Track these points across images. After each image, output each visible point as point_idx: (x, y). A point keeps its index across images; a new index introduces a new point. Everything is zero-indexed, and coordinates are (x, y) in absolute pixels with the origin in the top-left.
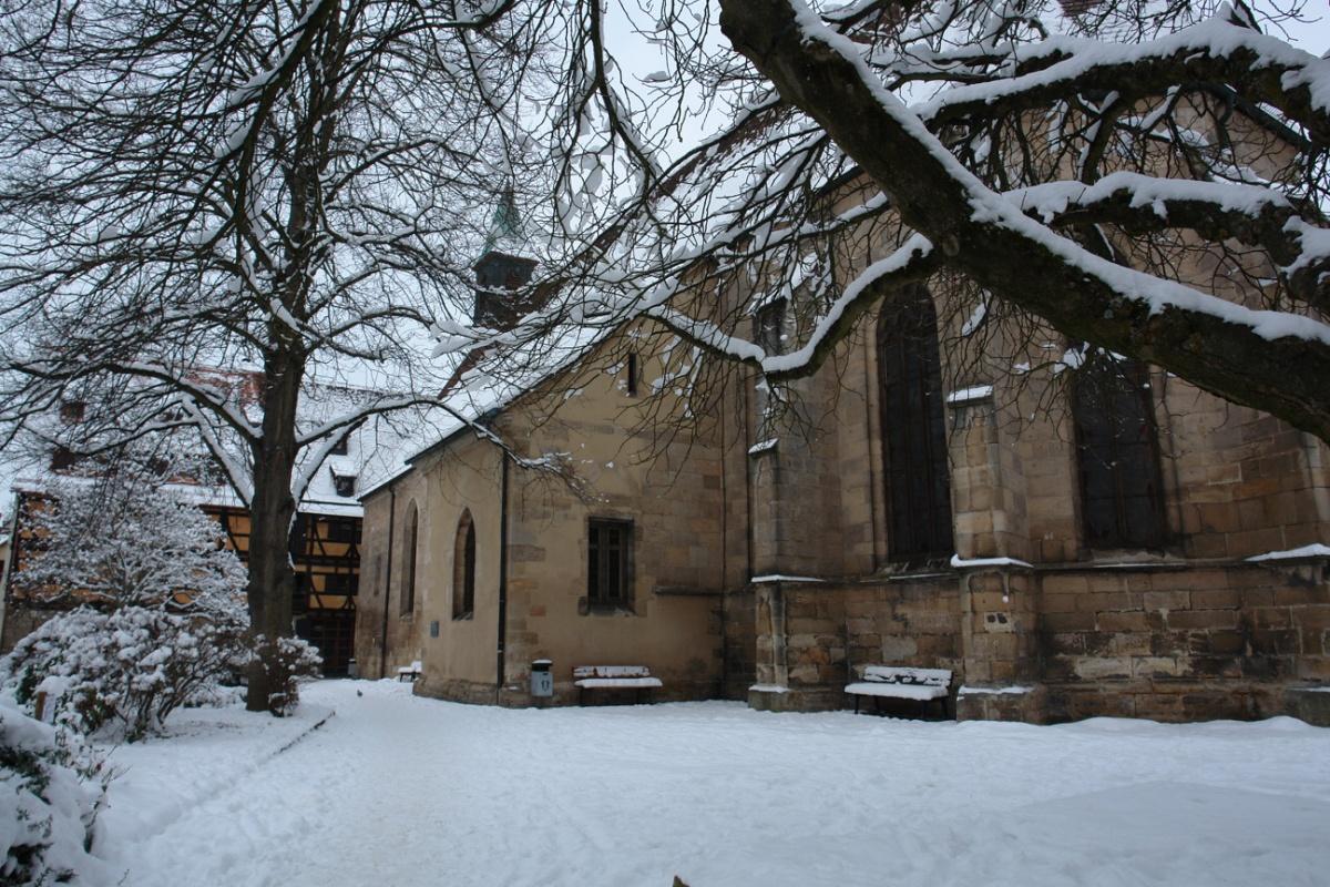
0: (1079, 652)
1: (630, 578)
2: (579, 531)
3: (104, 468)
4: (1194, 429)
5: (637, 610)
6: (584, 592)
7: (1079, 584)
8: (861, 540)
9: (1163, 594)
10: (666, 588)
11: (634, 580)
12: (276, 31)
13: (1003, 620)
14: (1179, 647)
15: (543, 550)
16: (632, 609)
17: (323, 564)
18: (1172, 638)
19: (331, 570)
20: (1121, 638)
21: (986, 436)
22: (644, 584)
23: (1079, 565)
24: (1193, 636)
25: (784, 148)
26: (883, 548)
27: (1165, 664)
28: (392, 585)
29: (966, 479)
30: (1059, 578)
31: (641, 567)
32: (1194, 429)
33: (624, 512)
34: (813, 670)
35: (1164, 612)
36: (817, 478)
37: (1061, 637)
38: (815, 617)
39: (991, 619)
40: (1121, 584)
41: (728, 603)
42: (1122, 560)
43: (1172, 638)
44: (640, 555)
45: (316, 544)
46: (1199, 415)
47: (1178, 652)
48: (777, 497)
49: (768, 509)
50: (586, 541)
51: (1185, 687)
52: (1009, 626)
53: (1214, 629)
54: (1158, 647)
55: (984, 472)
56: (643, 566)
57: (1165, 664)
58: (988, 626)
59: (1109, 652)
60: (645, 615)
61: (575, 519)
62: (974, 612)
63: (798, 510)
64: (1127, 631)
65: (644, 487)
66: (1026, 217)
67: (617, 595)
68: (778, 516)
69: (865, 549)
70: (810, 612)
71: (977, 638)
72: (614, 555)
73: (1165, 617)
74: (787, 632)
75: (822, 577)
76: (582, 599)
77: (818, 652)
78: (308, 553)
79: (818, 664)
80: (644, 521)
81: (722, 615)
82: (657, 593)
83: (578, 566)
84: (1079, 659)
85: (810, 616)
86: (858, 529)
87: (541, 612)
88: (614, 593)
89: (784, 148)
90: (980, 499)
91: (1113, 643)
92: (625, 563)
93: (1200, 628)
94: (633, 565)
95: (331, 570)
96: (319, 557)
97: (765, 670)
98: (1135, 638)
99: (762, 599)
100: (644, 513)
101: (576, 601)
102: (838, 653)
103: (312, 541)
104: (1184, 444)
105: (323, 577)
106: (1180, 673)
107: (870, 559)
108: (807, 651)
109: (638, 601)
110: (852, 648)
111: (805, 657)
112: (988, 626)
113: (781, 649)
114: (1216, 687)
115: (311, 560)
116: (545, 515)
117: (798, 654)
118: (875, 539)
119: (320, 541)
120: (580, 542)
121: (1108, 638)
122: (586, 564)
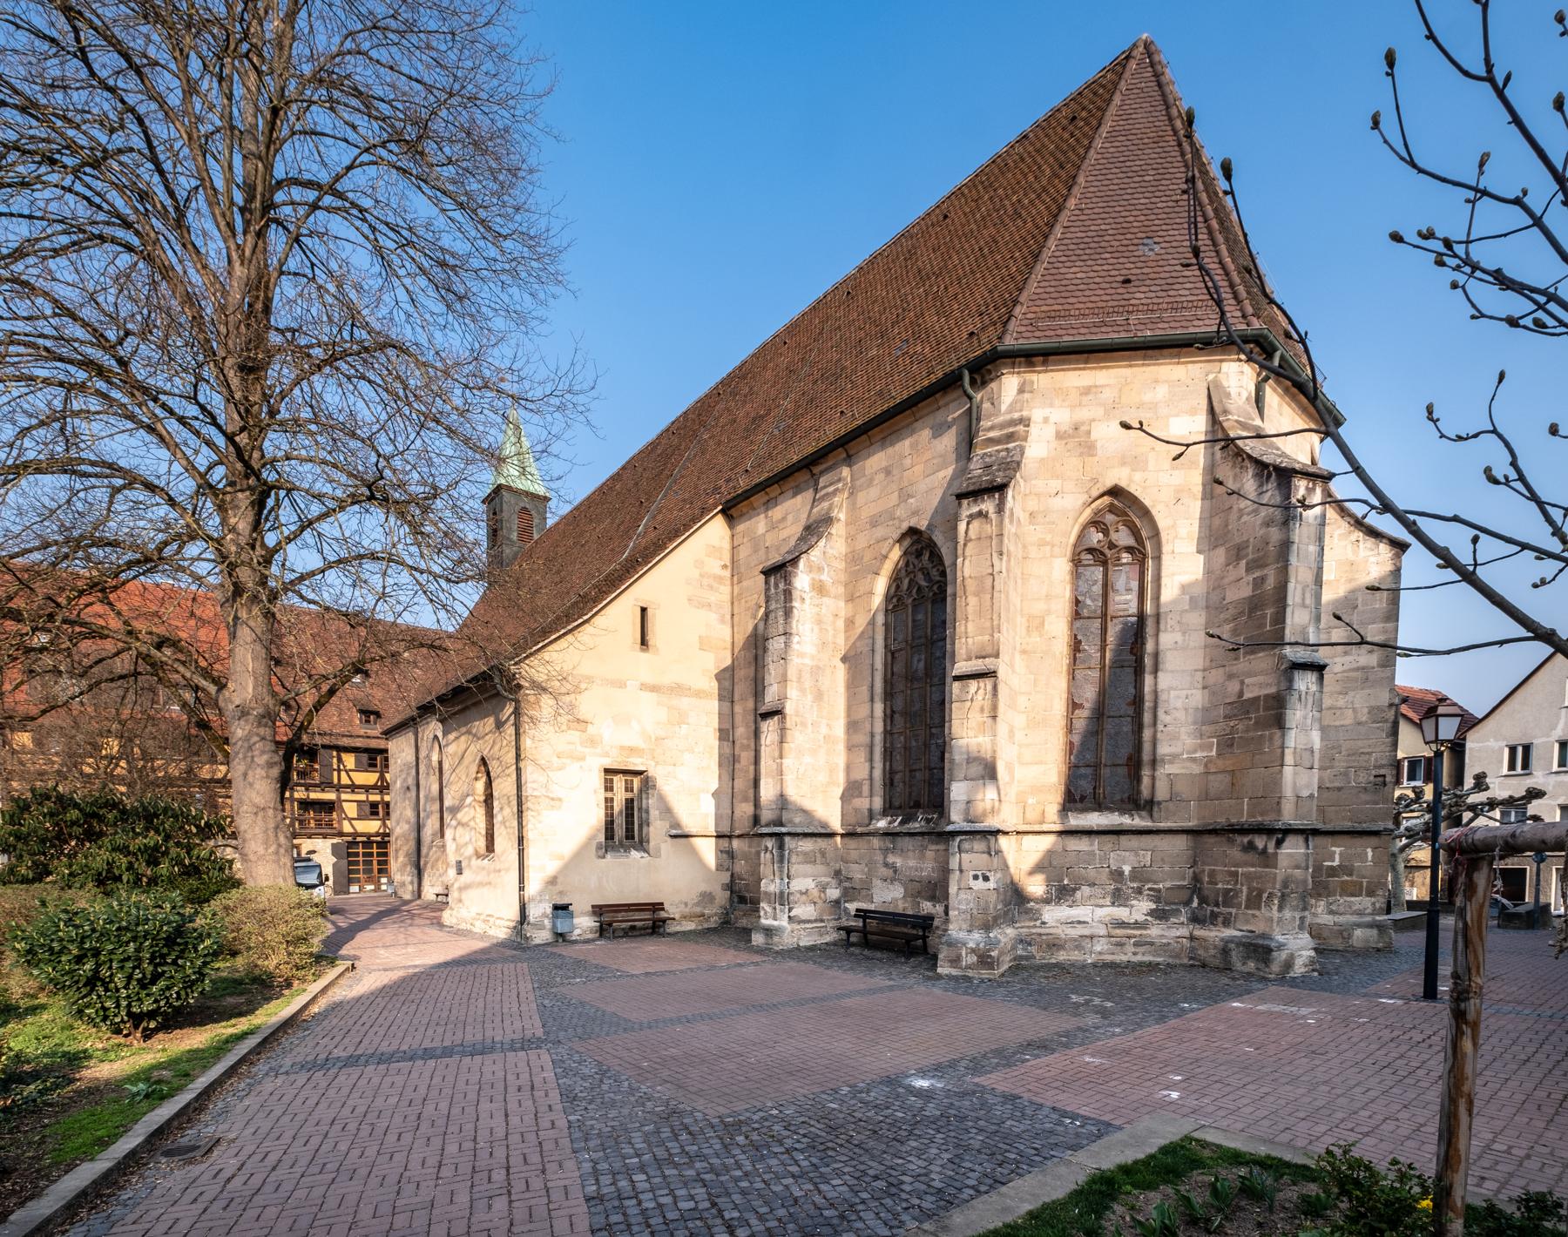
1: (645, 823)
16: (646, 851)
19: (363, 797)
20: (1086, 890)
27: (1122, 913)
32: (1179, 704)
35: (1127, 869)
39: (976, 877)
51: (1137, 932)
53: (1168, 884)
54: (1118, 898)
57: (1122, 913)
58: (972, 883)
60: (658, 856)
68: (943, 702)
77: (815, 893)
91: (1078, 894)
96: (347, 787)
98: (1098, 891)
109: (652, 844)
112: (972, 883)
121: (1075, 890)
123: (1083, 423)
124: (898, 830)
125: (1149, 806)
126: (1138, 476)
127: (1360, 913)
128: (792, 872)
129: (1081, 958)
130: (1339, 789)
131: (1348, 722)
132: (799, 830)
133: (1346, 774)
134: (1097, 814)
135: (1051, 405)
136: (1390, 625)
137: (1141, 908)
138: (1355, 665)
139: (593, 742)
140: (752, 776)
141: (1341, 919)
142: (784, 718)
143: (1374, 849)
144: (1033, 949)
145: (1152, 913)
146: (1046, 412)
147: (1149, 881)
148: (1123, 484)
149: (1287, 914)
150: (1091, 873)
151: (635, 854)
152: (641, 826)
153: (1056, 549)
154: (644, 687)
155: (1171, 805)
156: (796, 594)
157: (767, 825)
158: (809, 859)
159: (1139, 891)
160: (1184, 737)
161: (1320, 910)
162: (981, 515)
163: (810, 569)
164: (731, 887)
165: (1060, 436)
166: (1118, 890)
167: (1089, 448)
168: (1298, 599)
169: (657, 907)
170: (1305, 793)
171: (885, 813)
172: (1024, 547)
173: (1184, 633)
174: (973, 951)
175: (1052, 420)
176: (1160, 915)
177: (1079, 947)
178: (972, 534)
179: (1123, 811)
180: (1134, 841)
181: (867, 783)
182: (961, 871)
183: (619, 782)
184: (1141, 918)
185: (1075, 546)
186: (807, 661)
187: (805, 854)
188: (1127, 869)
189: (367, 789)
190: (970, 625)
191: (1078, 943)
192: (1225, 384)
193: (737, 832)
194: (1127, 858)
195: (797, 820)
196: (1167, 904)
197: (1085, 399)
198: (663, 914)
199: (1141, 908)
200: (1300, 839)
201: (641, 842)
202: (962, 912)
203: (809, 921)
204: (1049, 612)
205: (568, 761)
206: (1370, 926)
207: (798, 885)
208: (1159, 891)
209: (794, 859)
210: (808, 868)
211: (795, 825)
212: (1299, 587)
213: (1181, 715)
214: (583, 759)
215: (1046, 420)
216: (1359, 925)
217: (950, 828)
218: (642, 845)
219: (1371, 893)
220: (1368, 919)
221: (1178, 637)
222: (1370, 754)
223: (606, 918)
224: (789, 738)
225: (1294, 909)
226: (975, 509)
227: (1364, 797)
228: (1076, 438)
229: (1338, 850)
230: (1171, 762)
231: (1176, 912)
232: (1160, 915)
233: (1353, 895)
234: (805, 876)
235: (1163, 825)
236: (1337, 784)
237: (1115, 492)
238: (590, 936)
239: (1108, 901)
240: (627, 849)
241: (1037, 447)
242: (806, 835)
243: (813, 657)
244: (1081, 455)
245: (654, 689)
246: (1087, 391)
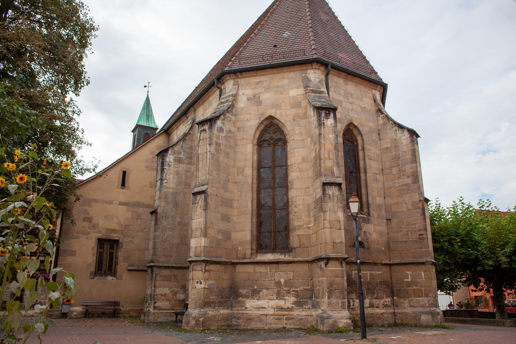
0: (248, 297)
4: (301, 203)
5: (117, 277)
6: (93, 269)
7: (250, 269)
9: (282, 273)
10: (133, 268)
13: (201, 283)
14: (287, 296)
15: (75, 252)
16: (115, 276)
18: (285, 292)
20: (265, 291)
21: (202, 207)
22: (122, 266)
23: (252, 260)
24: (293, 291)
27: (281, 303)
29: (195, 224)
30: (242, 266)
31: (120, 259)
32: (301, 203)
33: (114, 236)
35: (282, 281)
36: (177, 223)
37: (241, 291)
39: (197, 283)
40: (266, 269)
42: (269, 257)
43: (285, 292)
44: (121, 254)
46: (303, 197)
47: (287, 298)
51: (287, 313)
52: (202, 286)
53: (301, 288)
54: (279, 296)
55: (200, 222)
56: (122, 259)
57: (281, 303)
58: (196, 285)
59: (259, 297)
60: (121, 278)
64: (268, 289)
65: (125, 226)
67: (111, 271)
72: (111, 254)
73: (282, 283)
74: (155, 287)
77: (170, 295)
79: (170, 301)
84: (248, 300)
85: (168, 280)
90: (198, 233)
91: (261, 293)
93: (296, 288)
98: (270, 292)
100: (124, 236)
101: (89, 272)
104: (296, 210)
106: (286, 307)
111: (163, 297)
112: (196, 285)
113: (151, 294)
114: (308, 313)
117: (160, 296)
120: (93, 248)
121: (260, 291)
123: (257, 94)
125: (287, 249)
126: (278, 112)
127: (423, 306)
128: (157, 284)
129: (262, 326)
130: (405, 242)
131: (404, 209)
132: (161, 265)
133: (407, 234)
134: (270, 254)
135: (245, 89)
136: (414, 165)
137: (289, 301)
138: (403, 183)
139: (94, 227)
141: (415, 310)
142: (157, 214)
143: (425, 272)
144: (240, 321)
145: (295, 303)
146: (243, 91)
147: (292, 287)
148: (273, 115)
149: (334, 300)
150: (267, 283)
151: (110, 278)
152: (115, 265)
153: (248, 141)
154: (121, 203)
155: (300, 249)
156: (166, 164)
158: (167, 278)
159: (288, 292)
160: (303, 217)
161: (406, 305)
162: (204, 130)
163: (174, 153)
165: (248, 99)
166: (279, 291)
167: (259, 103)
168: (326, 156)
169: (116, 304)
170: (338, 241)
172: (236, 141)
173: (301, 172)
174: (194, 318)
175: (246, 94)
176: (299, 304)
177: (261, 321)
178: (201, 138)
179: (282, 253)
180: (285, 267)
182: (193, 279)
183: (107, 246)
184: (290, 306)
185: (258, 139)
186: (171, 190)
187: (165, 276)
188: (282, 281)
190: (200, 172)
191: (260, 318)
192: (309, 77)
194: (282, 275)
195: (161, 260)
196: (301, 298)
197: (257, 86)
199: (289, 301)
200: (338, 263)
201: (115, 273)
202: (193, 299)
203: (166, 309)
204: (246, 166)
205: (81, 235)
206: (428, 313)
207: (160, 291)
208: (297, 292)
209: (158, 278)
210: (167, 283)
211: (160, 262)
212: (327, 152)
213: (301, 208)
214: (89, 234)
215: (243, 94)
216: (423, 313)
218: (114, 274)
219: (427, 296)
220: (427, 309)
221: (298, 174)
222: (415, 224)
224: (158, 223)
225: (338, 298)
226: (202, 128)
227: (416, 245)
228: (255, 100)
229: (409, 273)
230: (299, 229)
231: (306, 303)
232: (299, 304)
233: (419, 297)
234: (165, 287)
235: (296, 259)
236: (404, 240)
237: (271, 118)
238: (79, 316)
239: (274, 297)
240: (106, 275)
241: (242, 103)
242: (165, 267)
243: (173, 189)
244: (257, 105)
245: (126, 204)
246: (258, 83)
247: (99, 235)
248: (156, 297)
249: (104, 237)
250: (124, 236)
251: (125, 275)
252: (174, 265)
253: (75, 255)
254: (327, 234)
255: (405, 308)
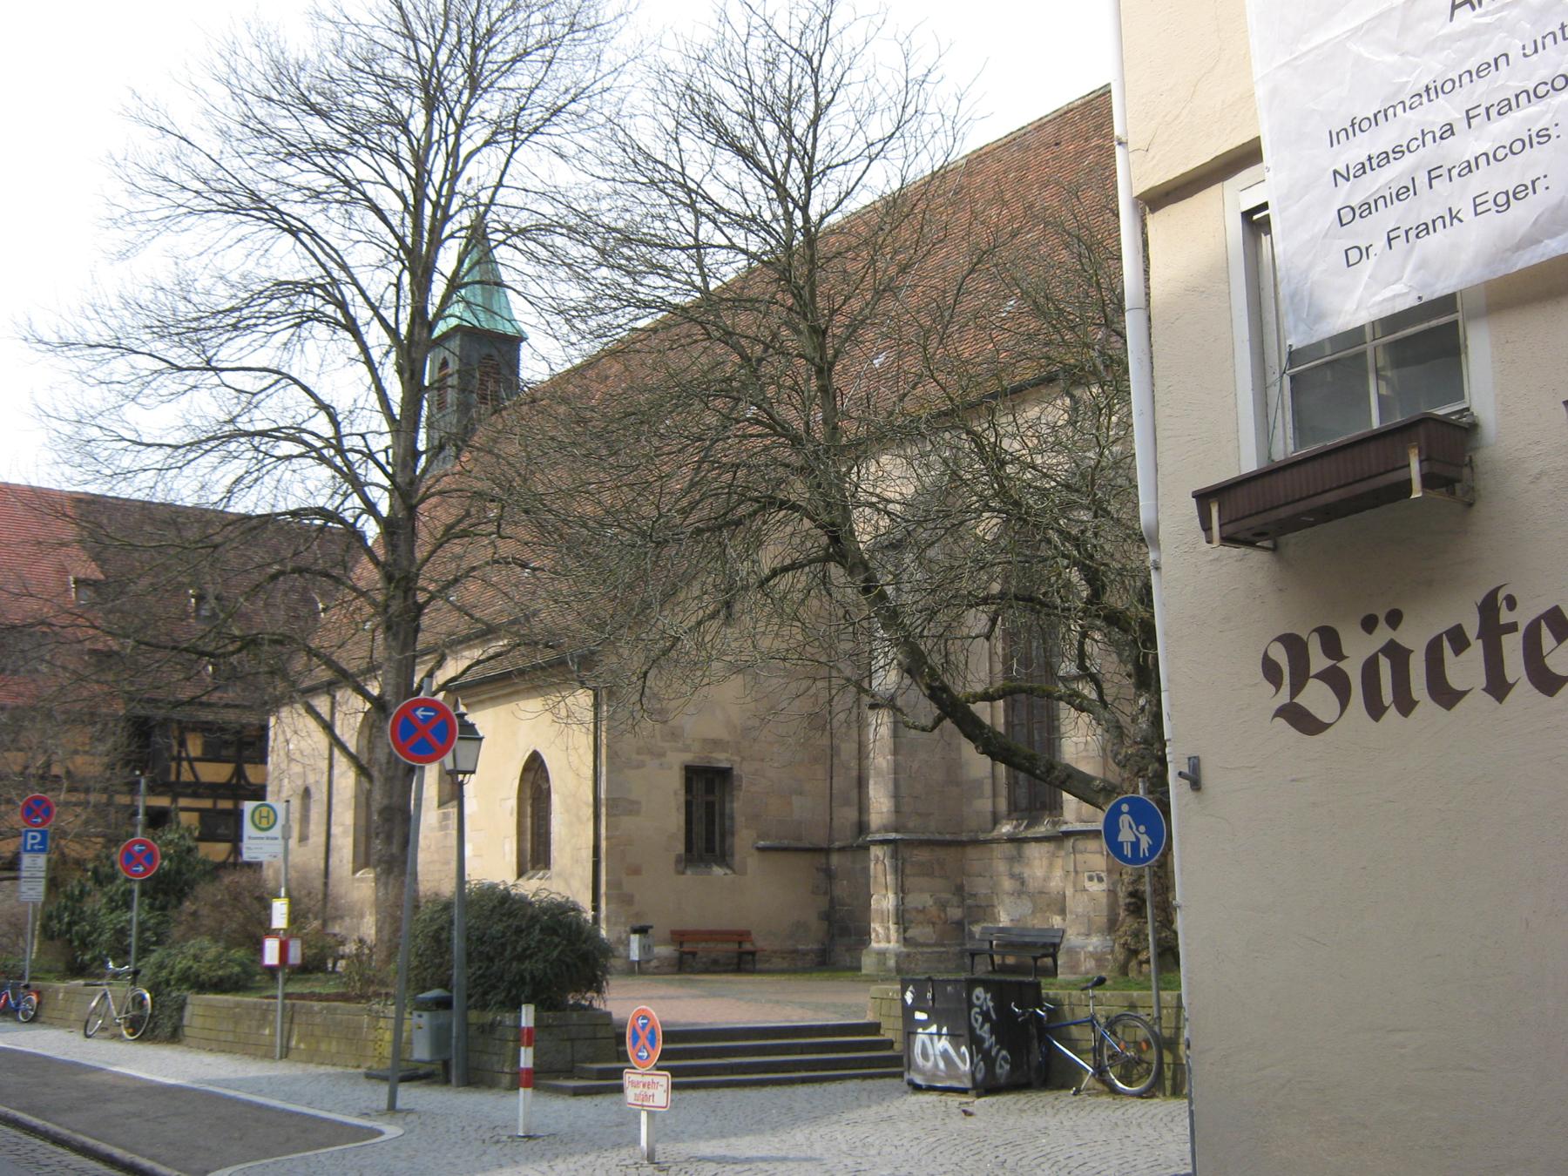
1: (727, 833)
2: (676, 781)
3: (35, 676)
6: (680, 848)
8: (981, 796)
11: (733, 834)
12: (696, 239)
13: (1100, 880)
15: (638, 803)
16: (729, 866)
17: (195, 795)
19: (207, 804)
22: (744, 839)
25: (333, 162)
26: (1003, 805)
28: (335, 830)
31: (740, 820)
33: (721, 759)
34: (929, 930)
38: (931, 875)
39: (1091, 879)
41: (835, 860)
44: (739, 806)
45: (185, 764)
48: (895, 752)
49: (885, 764)
50: (683, 792)
58: (1088, 884)
60: (744, 873)
61: (671, 768)
62: (1076, 872)
63: (915, 766)
66: (1492, 588)
67: (713, 850)
68: (895, 773)
69: (984, 805)
70: (927, 871)
71: (1078, 895)
72: (710, 806)
75: (896, 831)
76: (679, 856)
77: (934, 911)
78: (173, 778)
79: (934, 924)
80: (743, 770)
81: (829, 874)
82: (758, 849)
83: (675, 821)
86: (978, 783)
87: (636, 871)
88: (710, 848)
89: (333, 162)
92: (722, 815)
94: (732, 818)
95: (207, 804)
96: (188, 785)
97: (880, 930)
99: (877, 859)
100: (743, 759)
102: (955, 913)
103: (179, 760)
105: (195, 815)
107: (989, 817)
108: (923, 911)
109: (737, 858)
110: (970, 907)
111: (921, 917)
112: (1088, 884)
115: (175, 789)
116: (641, 765)
118: (995, 795)
119: (191, 761)
122: (682, 818)
124: (1023, 835)
139: (674, 735)
140: (854, 773)
151: (717, 871)
157: (878, 831)
164: (828, 916)
169: (742, 936)
171: (1009, 817)
174: (1091, 954)
181: (989, 781)
183: (699, 786)
189: (214, 790)
193: (837, 844)
198: (747, 946)
203: (928, 945)
214: (663, 755)
217: (1064, 828)
223: (687, 947)
240: (708, 864)
247: (688, 758)
248: (907, 916)
249: (698, 763)
250: (743, 759)
251: (753, 862)
252: (938, 837)
253: (637, 813)
254: (886, 719)
255: (130, 921)
